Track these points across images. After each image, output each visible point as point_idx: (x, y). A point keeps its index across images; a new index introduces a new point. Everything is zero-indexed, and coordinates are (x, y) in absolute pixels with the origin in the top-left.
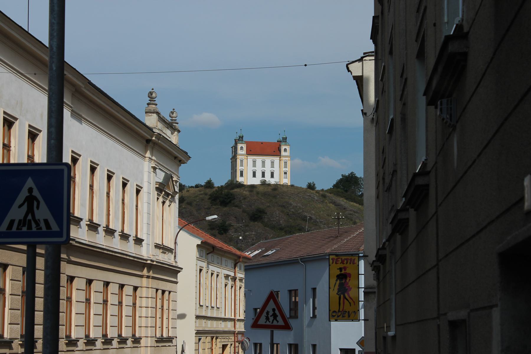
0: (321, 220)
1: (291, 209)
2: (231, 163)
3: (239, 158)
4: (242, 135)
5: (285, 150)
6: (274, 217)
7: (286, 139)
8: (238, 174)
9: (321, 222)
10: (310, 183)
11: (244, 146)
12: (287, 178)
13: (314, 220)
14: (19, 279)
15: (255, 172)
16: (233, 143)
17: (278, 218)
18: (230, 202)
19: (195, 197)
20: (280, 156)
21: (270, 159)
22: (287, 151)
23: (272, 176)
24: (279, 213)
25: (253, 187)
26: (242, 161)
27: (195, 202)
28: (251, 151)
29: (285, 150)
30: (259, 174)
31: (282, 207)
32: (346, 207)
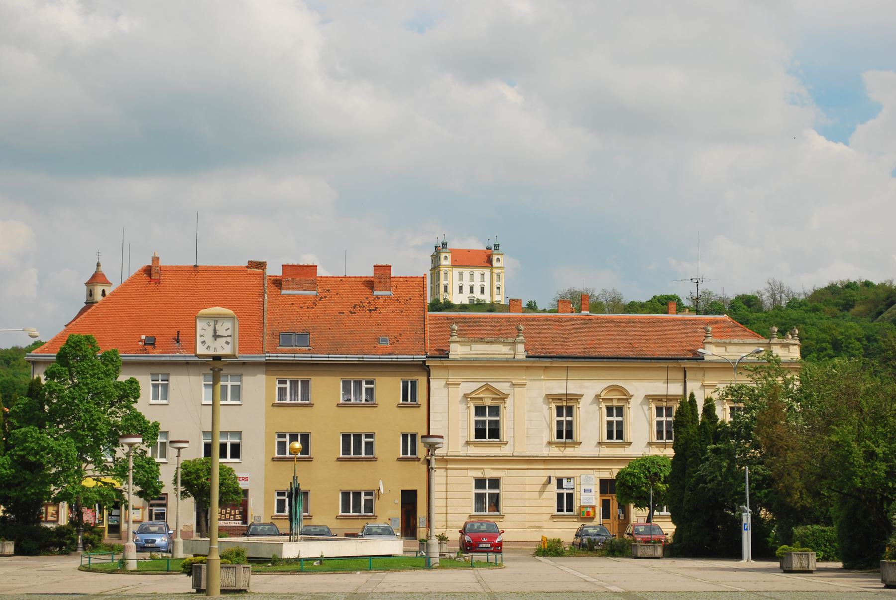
2: (431, 274)
3: (443, 270)
5: (446, 258)
8: (442, 289)
11: (449, 256)
14: (222, 407)
16: (432, 251)
23: (482, 292)
26: (446, 273)
29: (498, 260)
30: (466, 289)
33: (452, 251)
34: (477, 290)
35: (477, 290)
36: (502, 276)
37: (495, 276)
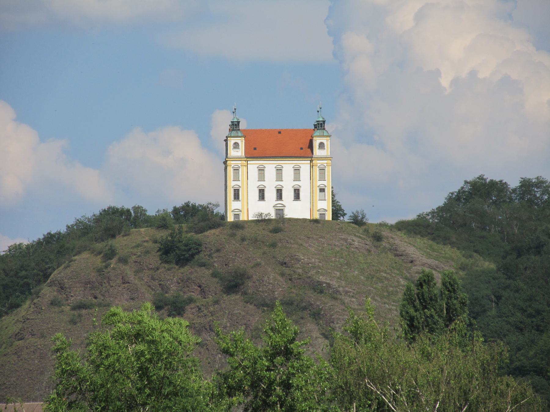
0: (347, 289)
1: (298, 268)
3: (232, 164)
4: (236, 120)
5: (236, 145)
6: (265, 285)
7: (324, 123)
9: (347, 292)
10: (357, 212)
11: (241, 142)
12: (326, 199)
13: (334, 288)
15: (299, 189)
17: (270, 287)
18: (193, 256)
19: (133, 248)
20: (312, 157)
21: (256, 164)
22: (240, 147)
24: (275, 277)
25: (262, 222)
26: (236, 170)
27: (134, 257)
28: (255, 149)
29: (322, 145)
30: (271, 194)
31: (282, 265)
32: (414, 259)
33: (246, 135)
34: (288, 194)
35: (288, 194)
36: (328, 172)
37: (230, 171)
